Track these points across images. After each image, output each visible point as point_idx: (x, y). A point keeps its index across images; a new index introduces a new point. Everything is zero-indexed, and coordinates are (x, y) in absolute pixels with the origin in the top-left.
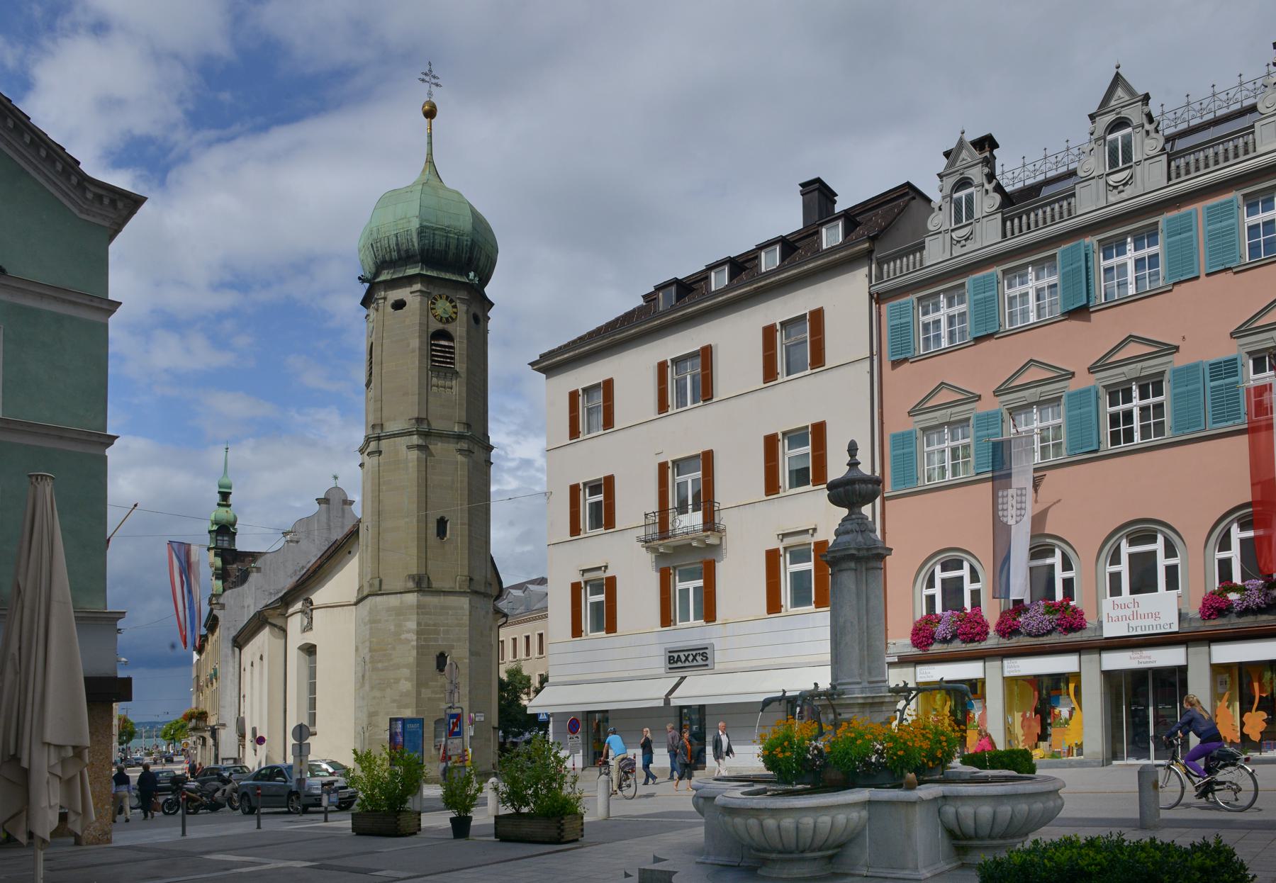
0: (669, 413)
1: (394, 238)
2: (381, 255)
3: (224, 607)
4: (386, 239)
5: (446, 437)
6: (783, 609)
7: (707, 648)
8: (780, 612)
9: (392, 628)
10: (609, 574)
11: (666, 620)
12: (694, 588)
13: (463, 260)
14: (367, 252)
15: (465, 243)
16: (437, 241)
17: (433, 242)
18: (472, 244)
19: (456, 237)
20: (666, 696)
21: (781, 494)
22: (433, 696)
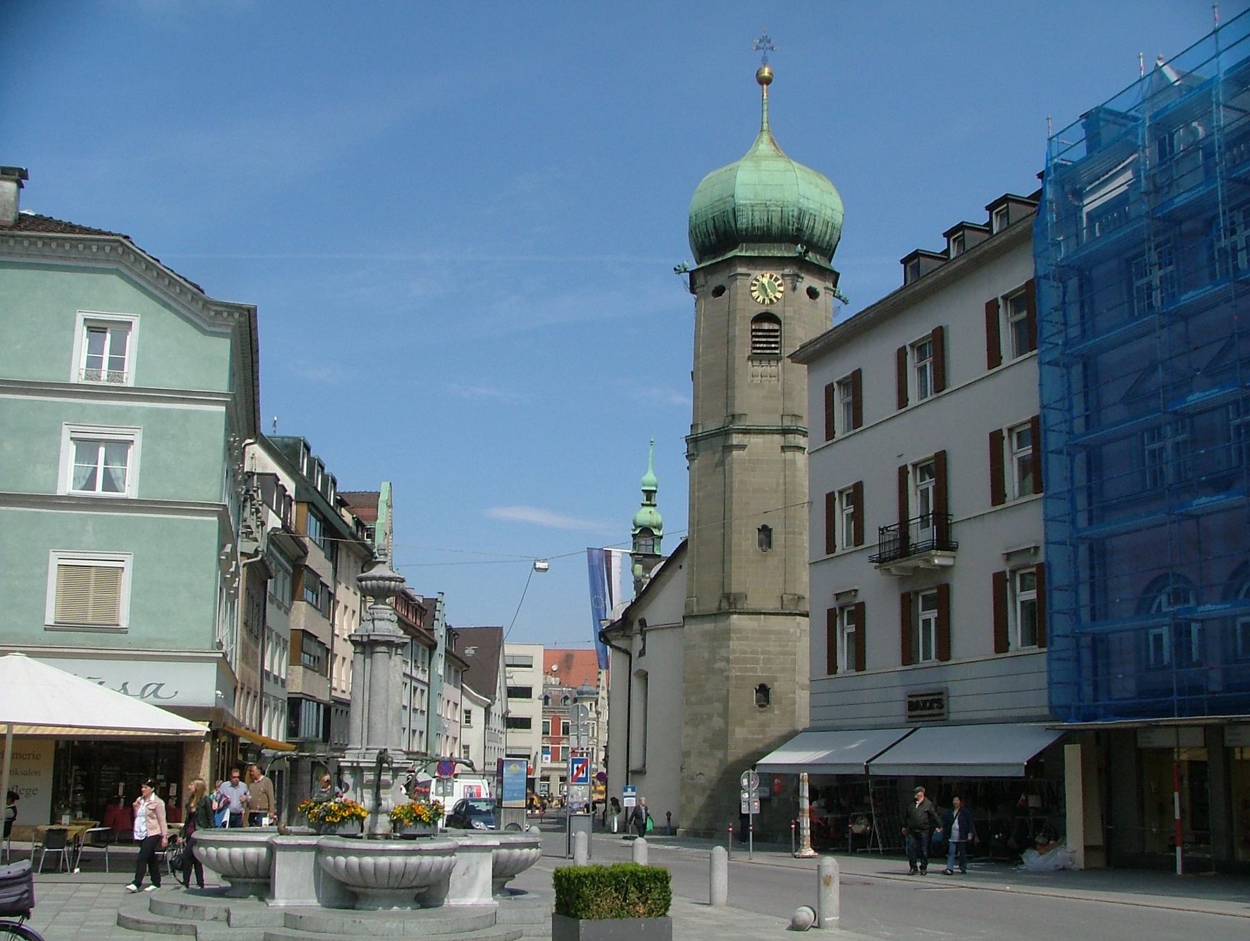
1: (712, 222)
6: (1011, 648)
7: (940, 694)
9: (706, 655)
11: (908, 656)
15: (791, 214)
16: (757, 218)
22: (750, 736)
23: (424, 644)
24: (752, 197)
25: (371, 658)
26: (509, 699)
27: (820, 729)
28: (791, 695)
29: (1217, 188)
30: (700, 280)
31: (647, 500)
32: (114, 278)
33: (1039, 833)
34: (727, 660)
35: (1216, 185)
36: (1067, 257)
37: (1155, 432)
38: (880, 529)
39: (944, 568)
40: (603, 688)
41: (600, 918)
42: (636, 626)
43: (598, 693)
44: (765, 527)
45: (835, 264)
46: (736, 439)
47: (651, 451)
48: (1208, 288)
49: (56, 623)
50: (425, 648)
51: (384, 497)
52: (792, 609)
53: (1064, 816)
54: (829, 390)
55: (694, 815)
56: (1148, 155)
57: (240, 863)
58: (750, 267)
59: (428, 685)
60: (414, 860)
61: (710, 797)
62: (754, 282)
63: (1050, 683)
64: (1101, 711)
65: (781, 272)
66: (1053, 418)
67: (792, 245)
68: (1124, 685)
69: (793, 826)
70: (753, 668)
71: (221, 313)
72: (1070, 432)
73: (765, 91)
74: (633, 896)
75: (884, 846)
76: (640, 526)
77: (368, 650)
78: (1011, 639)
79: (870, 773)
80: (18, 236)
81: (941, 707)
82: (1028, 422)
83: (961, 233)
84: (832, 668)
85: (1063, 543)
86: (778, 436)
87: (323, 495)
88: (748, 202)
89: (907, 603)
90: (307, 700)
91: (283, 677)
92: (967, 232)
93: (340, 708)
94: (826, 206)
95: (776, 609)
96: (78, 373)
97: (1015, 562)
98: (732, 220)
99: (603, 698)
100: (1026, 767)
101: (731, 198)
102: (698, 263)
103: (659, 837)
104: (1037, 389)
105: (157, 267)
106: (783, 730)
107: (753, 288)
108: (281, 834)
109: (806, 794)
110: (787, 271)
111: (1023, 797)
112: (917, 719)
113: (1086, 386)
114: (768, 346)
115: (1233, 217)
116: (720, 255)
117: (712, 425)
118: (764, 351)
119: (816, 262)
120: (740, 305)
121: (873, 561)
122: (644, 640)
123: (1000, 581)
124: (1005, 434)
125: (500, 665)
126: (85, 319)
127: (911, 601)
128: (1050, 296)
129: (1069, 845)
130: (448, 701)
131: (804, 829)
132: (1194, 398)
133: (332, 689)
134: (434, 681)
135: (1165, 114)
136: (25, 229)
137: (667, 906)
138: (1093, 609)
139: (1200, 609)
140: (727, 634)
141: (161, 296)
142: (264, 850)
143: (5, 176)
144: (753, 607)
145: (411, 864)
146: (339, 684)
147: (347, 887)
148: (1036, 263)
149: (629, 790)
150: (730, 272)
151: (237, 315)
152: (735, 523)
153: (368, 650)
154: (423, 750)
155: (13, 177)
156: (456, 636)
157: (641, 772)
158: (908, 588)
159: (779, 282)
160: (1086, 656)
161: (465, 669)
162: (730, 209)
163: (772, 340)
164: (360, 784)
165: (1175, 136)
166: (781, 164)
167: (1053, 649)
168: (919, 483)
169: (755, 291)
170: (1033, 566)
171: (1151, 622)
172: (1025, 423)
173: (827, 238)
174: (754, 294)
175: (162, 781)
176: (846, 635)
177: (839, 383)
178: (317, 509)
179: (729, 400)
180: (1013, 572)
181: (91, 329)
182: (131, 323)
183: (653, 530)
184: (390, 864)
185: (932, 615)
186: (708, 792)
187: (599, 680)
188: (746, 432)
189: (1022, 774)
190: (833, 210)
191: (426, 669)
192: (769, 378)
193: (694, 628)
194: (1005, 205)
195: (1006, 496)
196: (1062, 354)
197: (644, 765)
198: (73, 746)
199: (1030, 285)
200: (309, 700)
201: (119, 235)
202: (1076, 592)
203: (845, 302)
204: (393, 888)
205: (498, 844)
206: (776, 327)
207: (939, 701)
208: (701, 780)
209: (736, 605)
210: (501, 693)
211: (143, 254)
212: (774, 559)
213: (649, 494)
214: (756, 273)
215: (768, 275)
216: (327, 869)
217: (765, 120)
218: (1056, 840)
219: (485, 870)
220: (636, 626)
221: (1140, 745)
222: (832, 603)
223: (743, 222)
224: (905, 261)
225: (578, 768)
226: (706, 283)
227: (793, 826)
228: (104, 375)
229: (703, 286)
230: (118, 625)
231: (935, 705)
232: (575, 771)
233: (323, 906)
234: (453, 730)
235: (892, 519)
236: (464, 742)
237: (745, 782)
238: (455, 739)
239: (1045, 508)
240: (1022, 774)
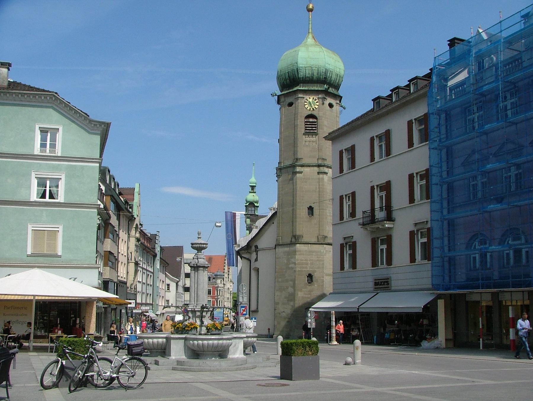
0: (356, 169)
1: (287, 74)
4: (284, 75)
5: (312, 167)
7: (388, 279)
8: (415, 262)
9: (286, 261)
10: (353, 240)
11: (374, 264)
15: (322, 71)
21: (416, 203)
22: (305, 296)
23: (151, 254)
25: (197, 272)
26: (186, 279)
27: (337, 293)
28: (322, 278)
29: (499, 85)
30: (282, 99)
31: (252, 190)
32: (51, 110)
33: (428, 334)
34: (295, 264)
35: (499, 83)
36: (441, 107)
37: (475, 178)
38: (363, 212)
39: (389, 228)
40: (226, 273)
41: (298, 356)
42: (253, 248)
43: (224, 275)
44: (310, 207)
45: (340, 92)
46: (298, 169)
47: (253, 168)
48: (495, 124)
49: (31, 253)
50: (152, 256)
51: (137, 190)
52: (322, 242)
53: (438, 327)
54: (341, 153)
55: (281, 329)
56: (474, 68)
57: (156, 344)
58: (304, 94)
59: (153, 273)
60: (221, 342)
61: (288, 322)
62: (306, 101)
63: (432, 276)
64: (452, 287)
65: (318, 97)
66: (434, 171)
67: (322, 85)
68: (461, 276)
69: (329, 333)
70: (306, 267)
71: (96, 125)
72: (441, 176)
73: (310, 15)
74: (308, 349)
75: (365, 341)
76: (248, 202)
77: (196, 269)
78: (416, 257)
79: (359, 311)
80: (11, 92)
81: (388, 284)
82: (424, 171)
83: (398, 90)
84: (342, 268)
85: (438, 221)
86: (316, 168)
87: (114, 190)
88: (304, 66)
89: (374, 242)
90: (111, 282)
91: (102, 272)
92: (400, 90)
93: (122, 284)
94: (337, 67)
95: (316, 242)
96: (37, 150)
97: (419, 227)
98: (296, 74)
99: (226, 278)
100: (423, 308)
101: (296, 64)
102: (281, 92)
103: (265, 339)
104: (428, 159)
105: (69, 106)
106: (318, 293)
107: (305, 104)
108: (172, 334)
109: (334, 320)
110: (320, 96)
111: (421, 320)
112: (378, 289)
113: (447, 159)
114: (312, 129)
115: (506, 94)
117: (288, 163)
118: (310, 131)
119: (332, 92)
120: (300, 111)
122: (257, 254)
123: (412, 235)
124: (415, 175)
125: (182, 263)
126: (39, 127)
127: (375, 241)
128: (433, 122)
129: (439, 339)
130: (160, 280)
131: (333, 334)
132: (489, 166)
133: (118, 276)
134: (156, 271)
135: (480, 53)
136: (12, 89)
137: (317, 352)
138: (449, 247)
139: (491, 248)
140: (295, 252)
141: (71, 117)
142: (165, 340)
143: (3, 66)
144: (305, 241)
146: (120, 274)
147: (196, 352)
148: (428, 107)
149: (254, 319)
150: (296, 96)
151: (103, 126)
152: (298, 205)
153: (196, 269)
154: (151, 303)
155: (6, 66)
156: (163, 250)
157: (256, 311)
158: (374, 236)
159: (317, 101)
160: (446, 265)
161: (167, 265)
162: (295, 69)
163: (314, 126)
164: (195, 316)
165: (485, 60)
166: (317, 49)
167: (434, 261)
168: (379, 193)
169: (306, 105)
170: (426, 229)
171: (472, 252)
172: (423, 171)
173: (337, 81)
174: (306, 106)
175: (73, 317)
176: (348, 254)
177: (345, 150)
178: (114, 199)
179: (295, 153)
180: (418, 231)
181: (41, 131)
182: (59, 129)
183: (255, 203)
184: (213, 343)
185: (384, 247)
186: (287, 320)
187: (224, 269)
188: (302, 166)
189: (421, 311)
190: (340, 69)
191: (150, 264)
192: (312, 143)
193: (280, 250)
194: (416, 80)
195: (415, 200)
196: (438, 145)
197: (257, 308)
198: (39, 304)
199: (426, 116)
200: (112, 282)
201: (53, 92)
202: (443, 240)
203: (344, 108)
204: (213, 352)
205: (245, 336)
206: (315, 120)
208: (284, 314)
209: (298, 240)
210: (183, 276)
211: (63, 100)
213: (253, 187)
214: (307, 97)
215: (312, 98)
216: (190, 346)
217: (310, 28)
218: (434, 337)
219: (240, 345)
220: (253, 248)
221: (467, 300)
222: (342, 241)
223: (301, 75)
224: (374, 100)
225: (243, 310)
226: (285, 100)
227: (329, 333)
228: (48, 151)
229: (283, 102)
230: (57, 254)
231: (386, 283)
232: (242, 311)
234: (162, 293)
235: (368, 208)
236: (167, 299)
237: (309, 315)
238: (163, 297)
239: (431, 206)
240: (421, 311)
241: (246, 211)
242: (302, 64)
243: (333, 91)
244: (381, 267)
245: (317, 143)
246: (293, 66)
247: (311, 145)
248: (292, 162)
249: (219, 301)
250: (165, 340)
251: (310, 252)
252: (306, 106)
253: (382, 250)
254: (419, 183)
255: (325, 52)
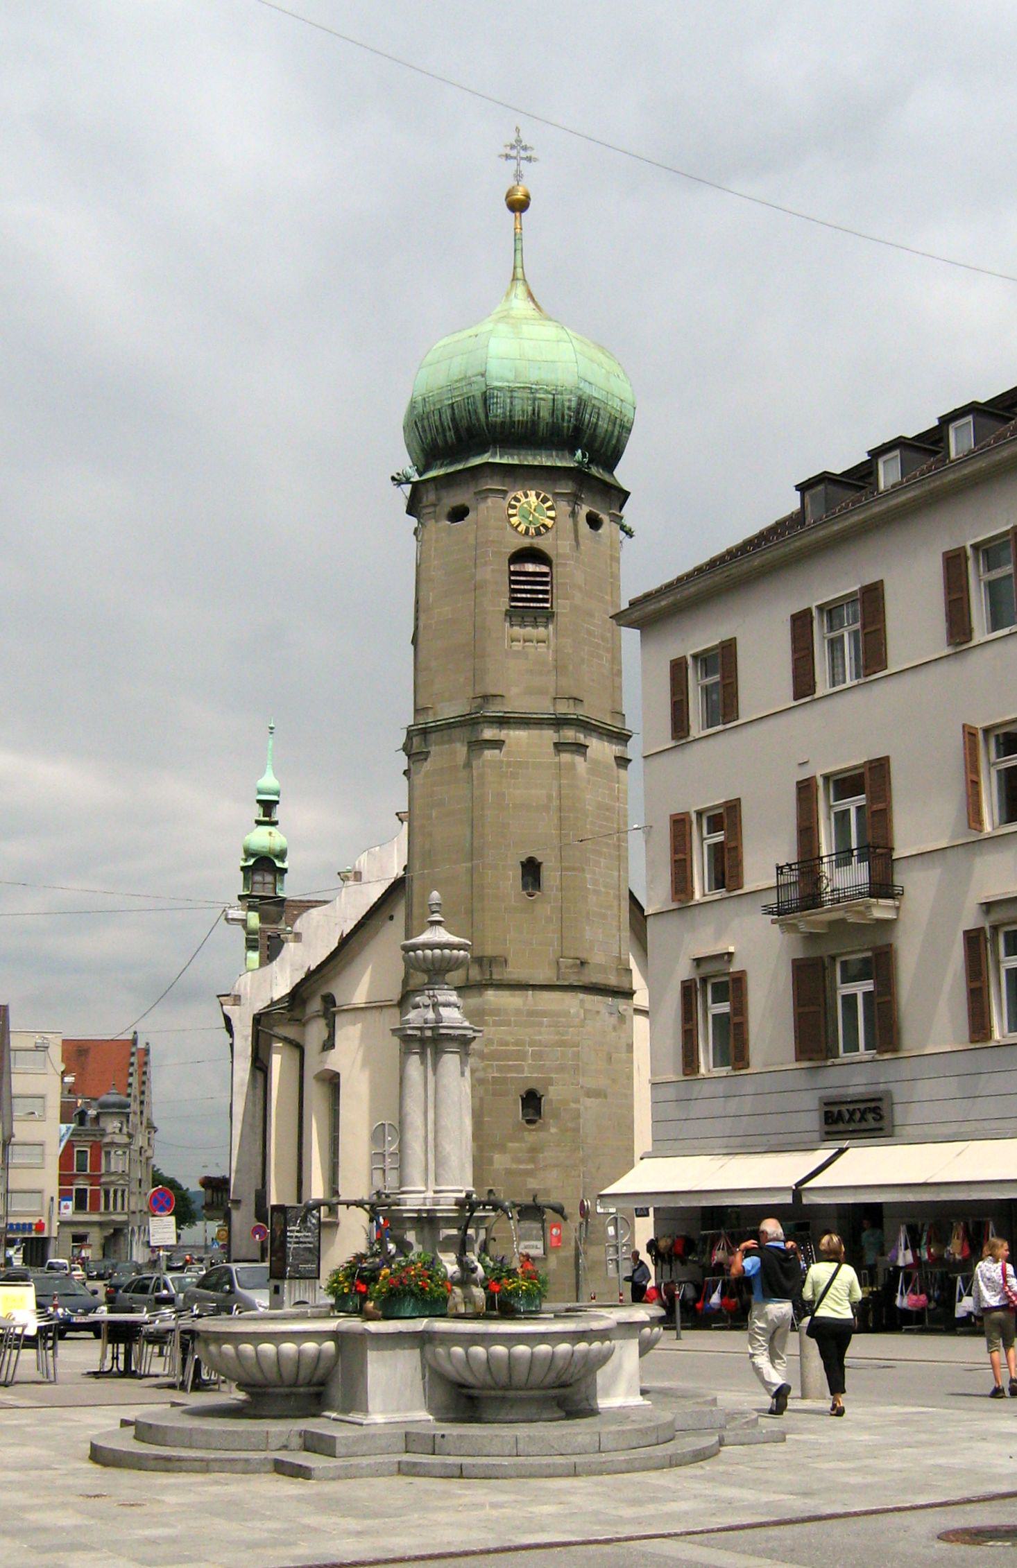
1: (449, 412)
2: (429, 438)
3: (240, 1000)
7: (880, 1099)
10: (733, 969)
12: (864, 993)
13: (565, 431)
14: (412, 435)
15: (567, 404)
16: (518, 408)
17: (510, 411)
18: (579, 404)
19: (551, 396)
20: (796, 1185)
22: (514, 1166)
24: (511, 377)
28: (573, 1105)
30: (429, 497)
31: (264, 816)
38: (778, 868)
40: (135, 1097)
52: (573, 980)
54: (678, 669)
58: (506, 479)
62: (513, 502)
81: (880, 1118)
84: (690, 1062)
88: (507, 384)
97: (998, 916)
98: (481, 410)
99: (135, 1113)
107: (511, 512)
114: (534, 596)
116: (458, 461)
117: (450, 710)
118: (528, 604)
121: (770, 913)
127: (824, 969)
145: (579, 1351)
159: (549, 504)
173: (614, 442)
179: (477, 675)
180: (995, 928)
183: (276, 861)
184: (553, 1352)
185: (861, 988)
187: (130, 1085)
190: (622, 400)
192: (535, 643)
206: (545, 569)
207: (876, 1110)
212: (545, 907)
213: (268, 806)
216: (448, 1367)
220: (316, 1005)
226: (439, 499)
233: (438, 1420)
235: (787, 852)
241: (246, 885)
242: (502, 379)
243: (599, 472)
244: (845, 1061)
245: (552, 644)
246: (470, 384)
247: (533, 650)
248: (469, 708)
249: (115, 1192)
250: (330, 1345)
251: (531, 1013)
252: (514, 520)
253: (850, 1000)
254: (995, 764)
255: (573, 340)
